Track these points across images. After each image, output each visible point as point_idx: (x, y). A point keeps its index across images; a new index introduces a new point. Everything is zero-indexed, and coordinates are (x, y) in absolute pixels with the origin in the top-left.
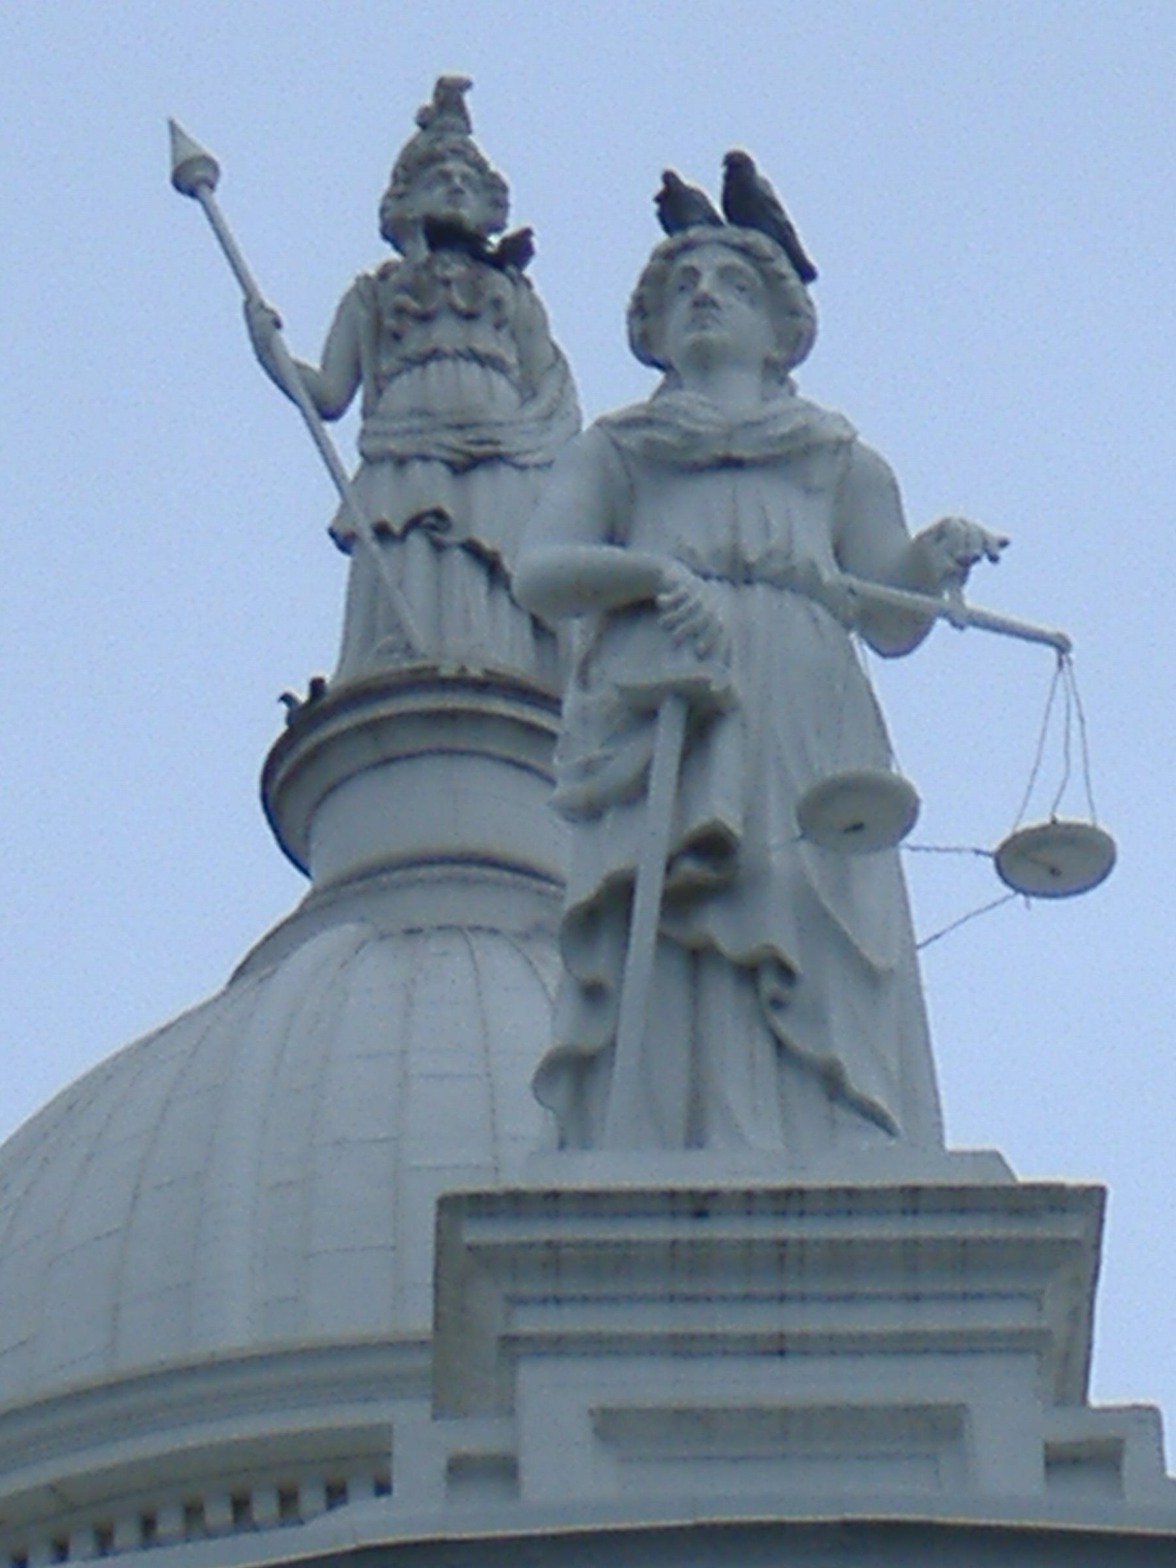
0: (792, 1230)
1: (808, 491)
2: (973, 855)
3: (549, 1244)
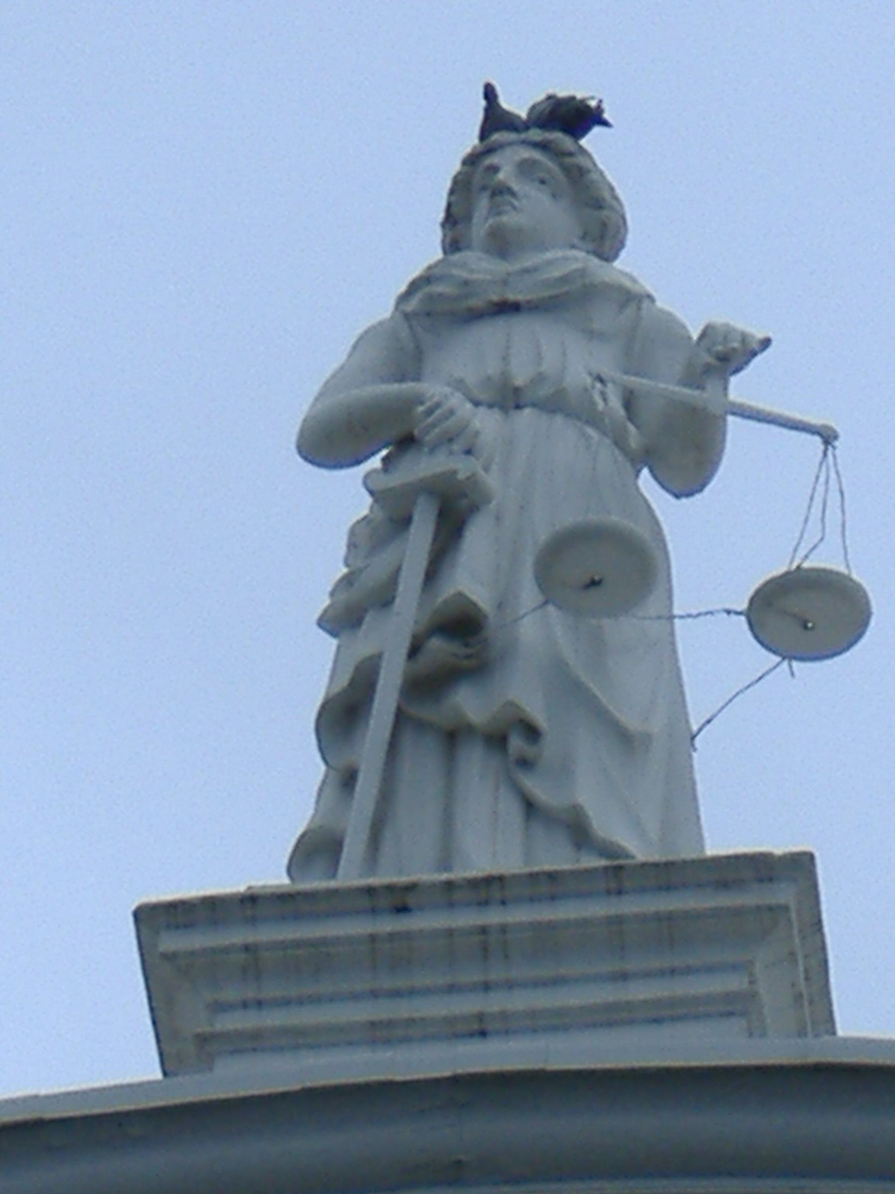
0: (494, 917)
1: (591, 335)
2: (725, 615)
3: (247, 948)
